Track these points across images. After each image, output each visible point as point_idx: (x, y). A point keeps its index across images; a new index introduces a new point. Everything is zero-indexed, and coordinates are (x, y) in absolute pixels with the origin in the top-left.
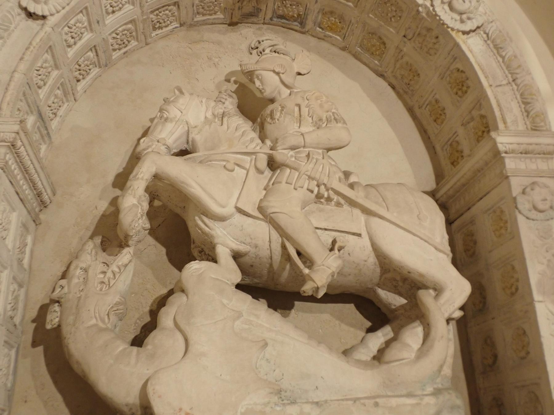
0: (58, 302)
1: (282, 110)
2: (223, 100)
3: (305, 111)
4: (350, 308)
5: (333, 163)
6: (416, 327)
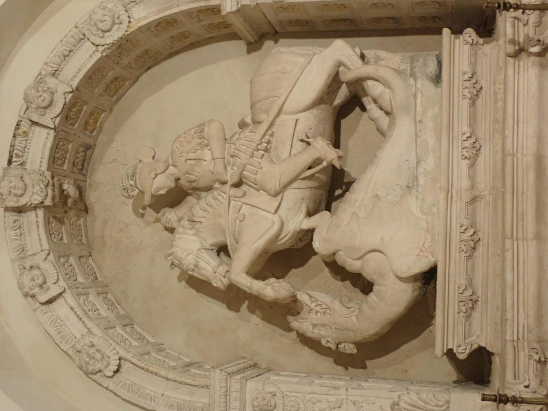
0: (338, 345)
1: (190, 174)
2: (168, 220)
3: (191, 156)
4: (345, 123)
5: (237, 136)
6: (367, 85)
